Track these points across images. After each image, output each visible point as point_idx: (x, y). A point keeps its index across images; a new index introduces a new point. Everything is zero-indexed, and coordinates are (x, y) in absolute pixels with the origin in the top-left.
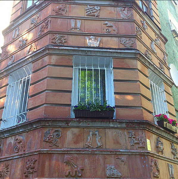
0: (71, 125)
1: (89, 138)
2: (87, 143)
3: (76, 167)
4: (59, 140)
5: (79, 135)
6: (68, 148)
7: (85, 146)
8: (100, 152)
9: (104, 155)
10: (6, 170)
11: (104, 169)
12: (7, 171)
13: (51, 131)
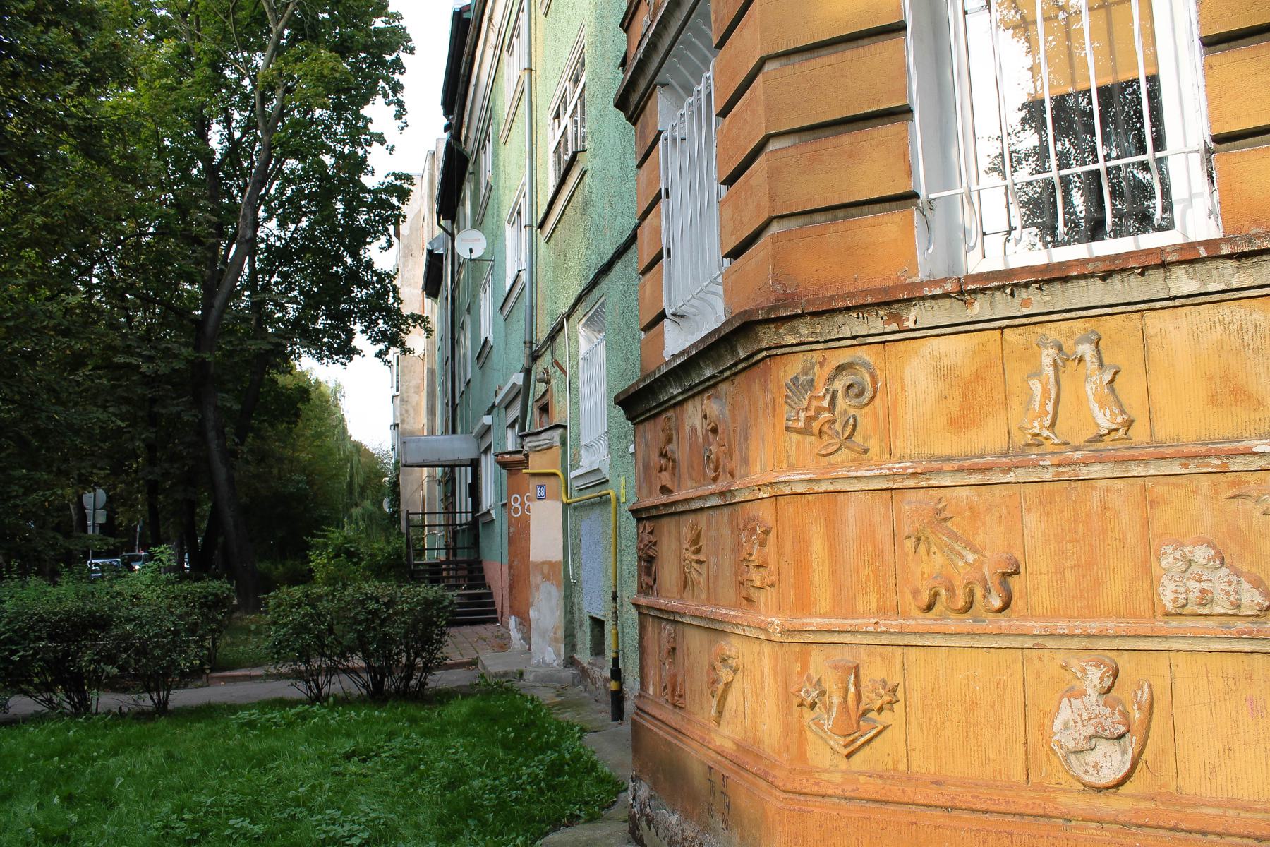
0: (918, 326)
1: (1036, 386)
2: (1026, 423)
3: (971, 557)
4: (865, 415)
5: (977, 377)
6: (919, 459)
7: (1019, 439)
8: (1111, 466)
9: (1140, 481)
10: (694, 557)
11: (1146, 569)
12: (698, 562)
13: (816, 368)
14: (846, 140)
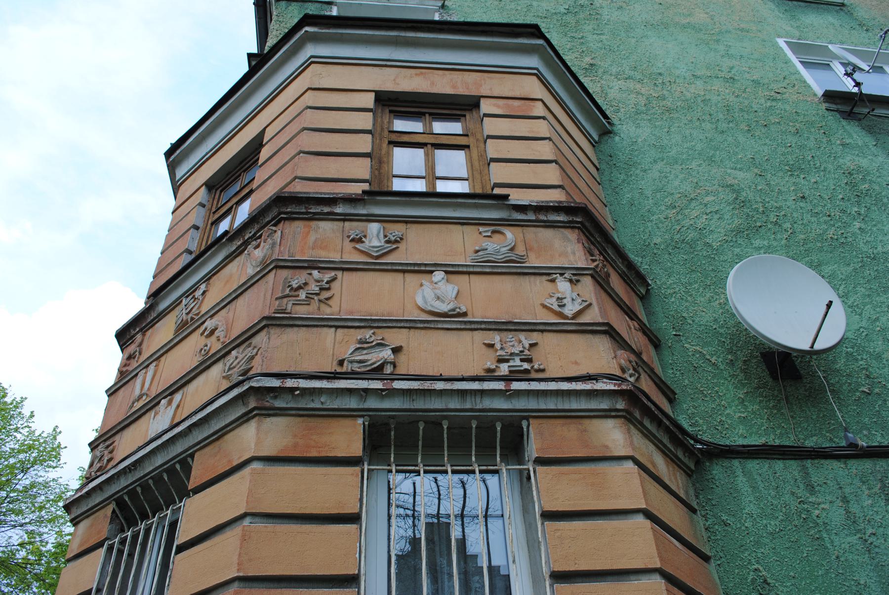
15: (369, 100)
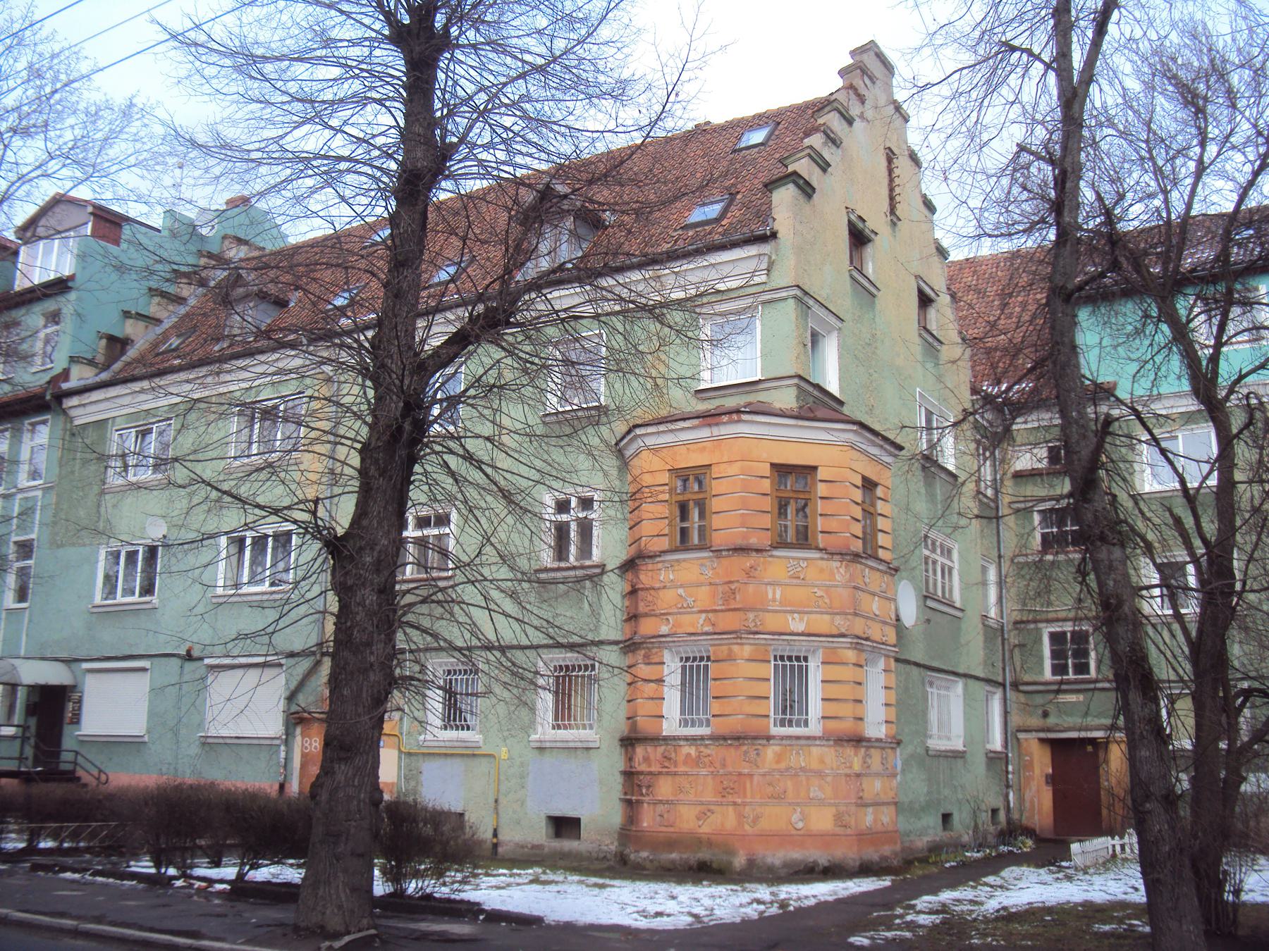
14: (757, 701)
15: (767, 472)
